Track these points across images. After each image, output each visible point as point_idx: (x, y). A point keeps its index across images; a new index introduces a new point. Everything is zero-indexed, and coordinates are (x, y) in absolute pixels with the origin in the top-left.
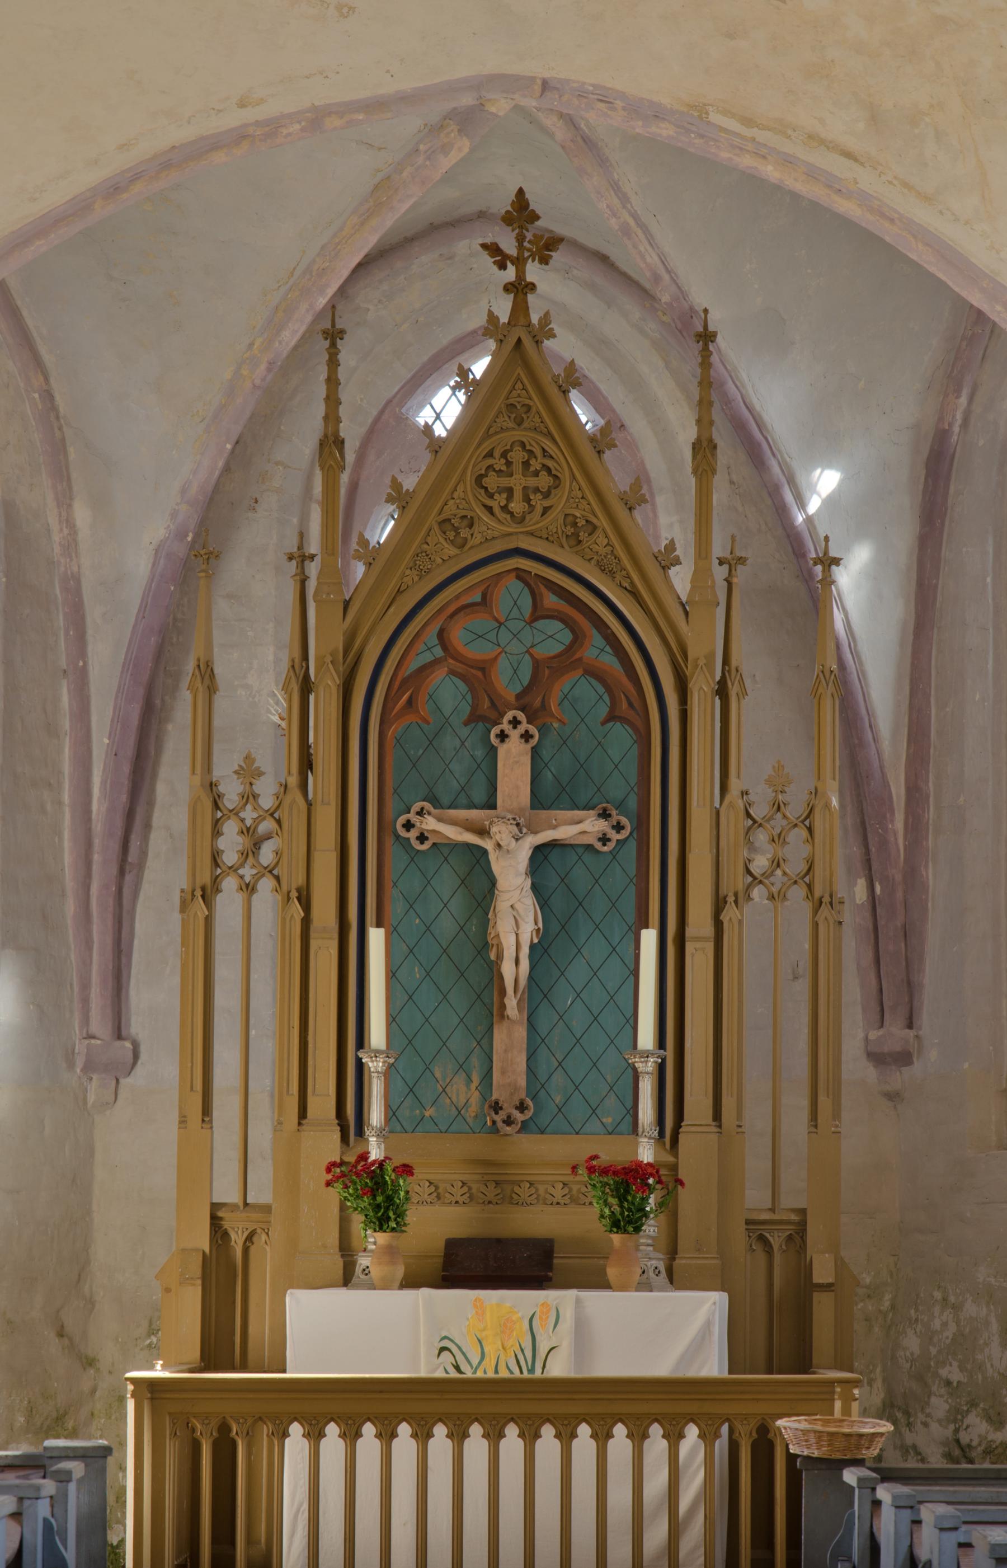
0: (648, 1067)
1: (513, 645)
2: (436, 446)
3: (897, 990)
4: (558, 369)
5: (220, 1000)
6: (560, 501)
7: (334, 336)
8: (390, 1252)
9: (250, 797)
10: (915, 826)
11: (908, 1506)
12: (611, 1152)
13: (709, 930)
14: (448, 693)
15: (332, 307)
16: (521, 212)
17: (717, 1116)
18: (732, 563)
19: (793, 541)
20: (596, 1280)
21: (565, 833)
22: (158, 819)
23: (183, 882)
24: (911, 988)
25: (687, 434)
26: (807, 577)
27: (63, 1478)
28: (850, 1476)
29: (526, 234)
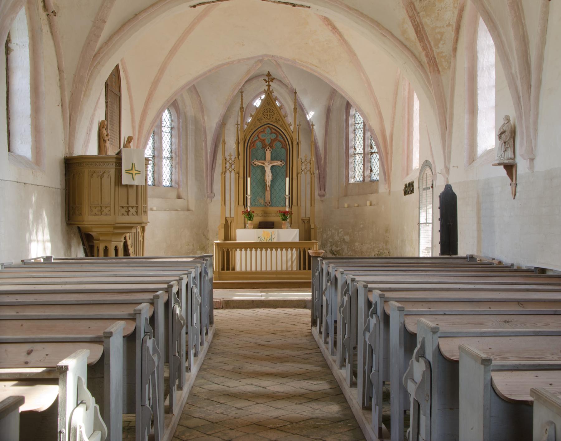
0: (288, 197)
1: (268, 137)
2: (257, 108)
3: (323, 185)
4: (274, 97)
5: (227, 187)
6: (275, 116)
7: (242, 92)
8: (251, 224)
9: (230, 159)
10: (325, 162)
11: (328, 264)
12: (282, 209)
13: (296, 178)
14: (259, 144)
15: (242, 88)
16: (269, 75)
17: (297, 204)
18: (299, 125)
19: (308, 122)
20: (280, 227)
21: (275, 164)
22: (217, 162)
23: (221, 171)
24: (324, 185)
25: (293, 107)
26: (310, 127)
27: (207, 260)
28: (319, 259)
29: (270, 78)
